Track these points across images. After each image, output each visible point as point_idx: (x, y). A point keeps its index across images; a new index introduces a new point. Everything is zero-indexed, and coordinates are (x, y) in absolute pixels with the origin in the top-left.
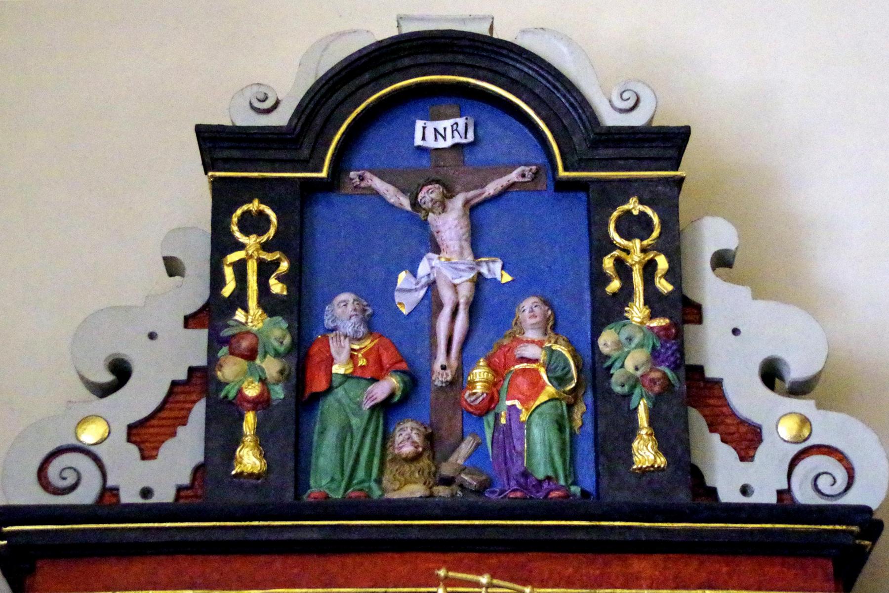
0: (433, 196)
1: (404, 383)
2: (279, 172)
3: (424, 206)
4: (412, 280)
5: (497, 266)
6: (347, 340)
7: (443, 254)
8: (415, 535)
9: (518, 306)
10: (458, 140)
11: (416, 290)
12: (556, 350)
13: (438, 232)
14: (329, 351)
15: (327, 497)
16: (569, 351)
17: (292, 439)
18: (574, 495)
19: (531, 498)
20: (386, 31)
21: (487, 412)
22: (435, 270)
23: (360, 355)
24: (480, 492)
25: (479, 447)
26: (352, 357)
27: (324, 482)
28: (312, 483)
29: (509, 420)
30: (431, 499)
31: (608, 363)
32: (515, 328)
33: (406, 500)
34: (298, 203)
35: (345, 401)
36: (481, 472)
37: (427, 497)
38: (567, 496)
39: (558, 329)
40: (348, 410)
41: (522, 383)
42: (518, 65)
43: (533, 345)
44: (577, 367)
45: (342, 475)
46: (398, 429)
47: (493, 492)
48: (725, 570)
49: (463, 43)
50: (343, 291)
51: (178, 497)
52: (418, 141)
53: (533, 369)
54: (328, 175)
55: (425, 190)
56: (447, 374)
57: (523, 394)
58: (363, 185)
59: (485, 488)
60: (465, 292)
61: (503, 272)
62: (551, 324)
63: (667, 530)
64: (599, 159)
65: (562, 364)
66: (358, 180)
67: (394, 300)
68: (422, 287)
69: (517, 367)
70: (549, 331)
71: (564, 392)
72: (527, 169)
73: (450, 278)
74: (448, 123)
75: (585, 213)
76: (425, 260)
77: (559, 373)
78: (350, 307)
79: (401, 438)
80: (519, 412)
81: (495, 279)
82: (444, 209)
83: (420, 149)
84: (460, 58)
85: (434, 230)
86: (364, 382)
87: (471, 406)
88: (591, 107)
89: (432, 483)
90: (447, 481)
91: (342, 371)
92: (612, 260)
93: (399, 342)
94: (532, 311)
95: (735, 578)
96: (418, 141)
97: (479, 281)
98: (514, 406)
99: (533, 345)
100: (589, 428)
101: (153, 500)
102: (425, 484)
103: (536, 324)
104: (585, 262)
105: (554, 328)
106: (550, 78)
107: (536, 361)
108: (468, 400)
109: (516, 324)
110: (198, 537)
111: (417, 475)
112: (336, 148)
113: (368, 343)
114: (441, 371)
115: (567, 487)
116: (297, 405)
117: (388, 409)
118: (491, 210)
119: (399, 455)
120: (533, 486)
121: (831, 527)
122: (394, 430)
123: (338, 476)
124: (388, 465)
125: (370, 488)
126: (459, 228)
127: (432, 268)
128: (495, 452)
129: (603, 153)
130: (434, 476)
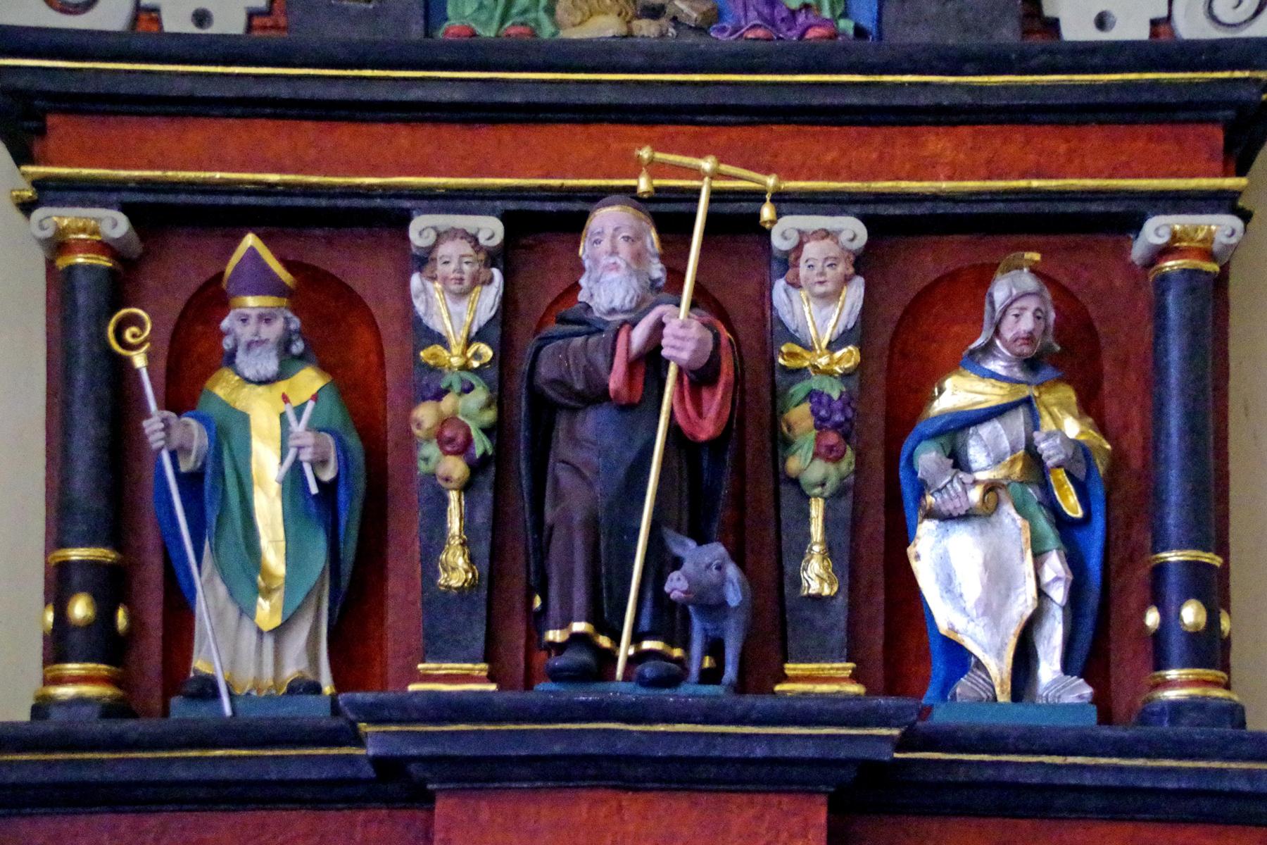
8: (605, 97)
15: (474, 35)
18: (844, 34)
24: (700, 29)
27: (468, 11)
30: (630, 40)
38: (834, 36)
47: (723, 30)
48: (1063, 148)
51: (249, 27)
59: (710, 24)
63: (982, 88)
95: (1077, 162)
101: (213, 30)
102: (619, 15)
104: (1232, 566)
110: (285, 92)
115: (833, 21)
120: (783, 20)
121: (1226, 75)
125: (536, 20)
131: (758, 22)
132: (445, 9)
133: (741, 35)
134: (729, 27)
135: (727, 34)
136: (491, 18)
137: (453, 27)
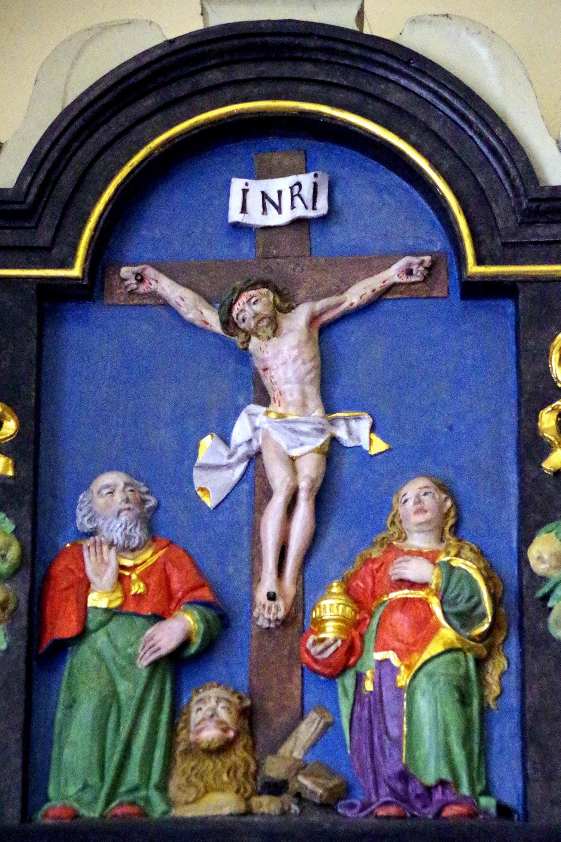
0: (257, 308)
1: (206, 621)
2: (24, 268)
3: (242, 326)
4: (222, 448)
5: (363, 426)
6: (113, 550)
7: (274, 407)
9: (397, 492)
10: (300, 212)
11: (229, 466)
12: (459, 568)
13: (265, 370)
14: (83, 569)
15: (76, 816)
16: (479, 569)
17: (19, 720)
18: (486, 812)
19: (413, 816)
20: (182, 21)
21: (344, 669)
22: (260, 433)
23: (134, 577)
24: (327, 806)
25: (330, 727)
26: (121, 579)
27: (72, 791)
28: (51, 791)
29: (378, 683)
30: (248, 819)
31: (545, 589)
32: (392, 530)
33: (204, 820)
34: (33, 322)
35: (108, 653)
36: (331, 772)
37: (240, 815)
39: (463, 532)
40: (114, 669)
41: (401, 622)
42: (403, 82)
43: (421, 557)
44: (493, 596)
45: (102, 778)
46: (196, 699)
47: (352, 806)
49: (311, 43)
50: (110, 469)
52: (235, 215)
53: (420, 600)
54: (84, 272)
55: (244, 298)
56: (277, 609)
57: (402, 641)
58: (142, 289)
60: (309, 469)
61: (373, 436)
62: (451, 522)
64: (536, 243)
65: (466, 594)
66: (134, 281)
67: (192, 483)
68: (240, 461)
69: (392, 595)
70: (448, 536)
71: (473, 639)
72: (416, 260)
73: (285, 447)
74: (284, 183)
75: (512, 334)
76: (243, 416)
77: (462, 606)
78: (118, 497)
79: (200, 715)
80: (395, 671)
81: (360, 447)
82: (276, 331)
83: (237, 226)
84: (308, 70)
85: (259, 365)
86: (139, 622)
87: (316, 661)
88: (524, 153)
89: (249, 789)
90: (276, 788)
91: (103, 603)
92: (555, 415)
93: (196, 556)
94: (418, 501)
96: (235, 215)
97: (332, 451)
98: (387, 661)
99: (421, 557)
100: (513, 700)
102: (237, 792)
103: (427, 522)
104: (510, 415)
105: (456, 529)
106: (457, 103)
107: (424, 585)
108: (313, 651)
109: (393, 523)
111: (225, 778)
112: (96, 229)
113: (148, 557)
114: (268, 603)
116: (28, 661)
117: (180, 667)
118: (355, 331)
119: (197, 744)
120: (418, 796)
122: (190, 700)
123: (94, 780)
124: (179, 759)
125: (147, 800)
126: (299, 362)
127: (256, 429)
128: (356, 737)
129: (544, 232)
130: (255, 779)
131: (389, 799)
132: (46, 788)
133: (371, 813)
134: (358, 803)
135: (355, 811)
136: (96, 799)
137: (54, 808)
